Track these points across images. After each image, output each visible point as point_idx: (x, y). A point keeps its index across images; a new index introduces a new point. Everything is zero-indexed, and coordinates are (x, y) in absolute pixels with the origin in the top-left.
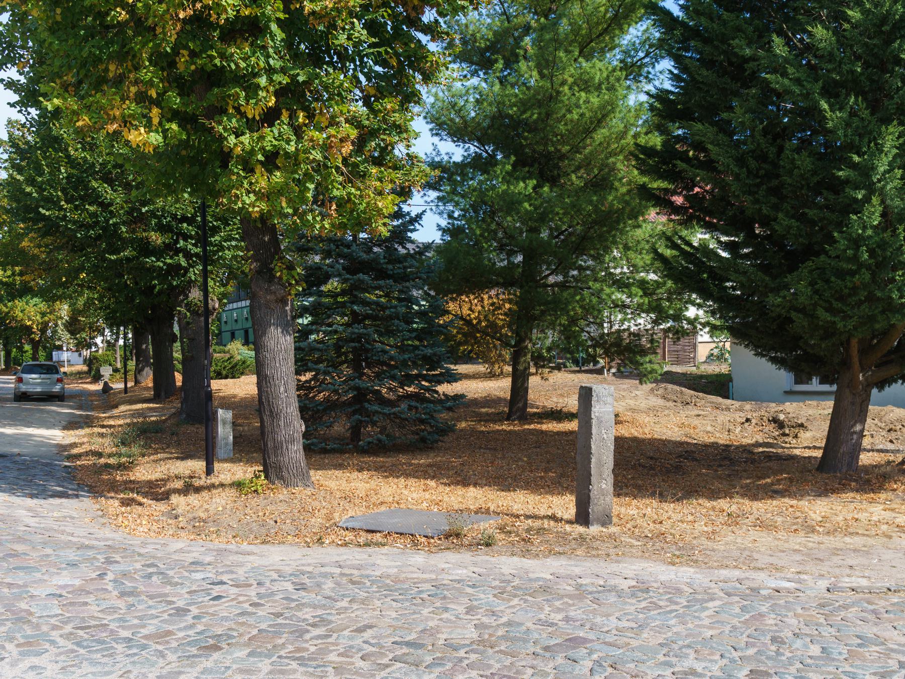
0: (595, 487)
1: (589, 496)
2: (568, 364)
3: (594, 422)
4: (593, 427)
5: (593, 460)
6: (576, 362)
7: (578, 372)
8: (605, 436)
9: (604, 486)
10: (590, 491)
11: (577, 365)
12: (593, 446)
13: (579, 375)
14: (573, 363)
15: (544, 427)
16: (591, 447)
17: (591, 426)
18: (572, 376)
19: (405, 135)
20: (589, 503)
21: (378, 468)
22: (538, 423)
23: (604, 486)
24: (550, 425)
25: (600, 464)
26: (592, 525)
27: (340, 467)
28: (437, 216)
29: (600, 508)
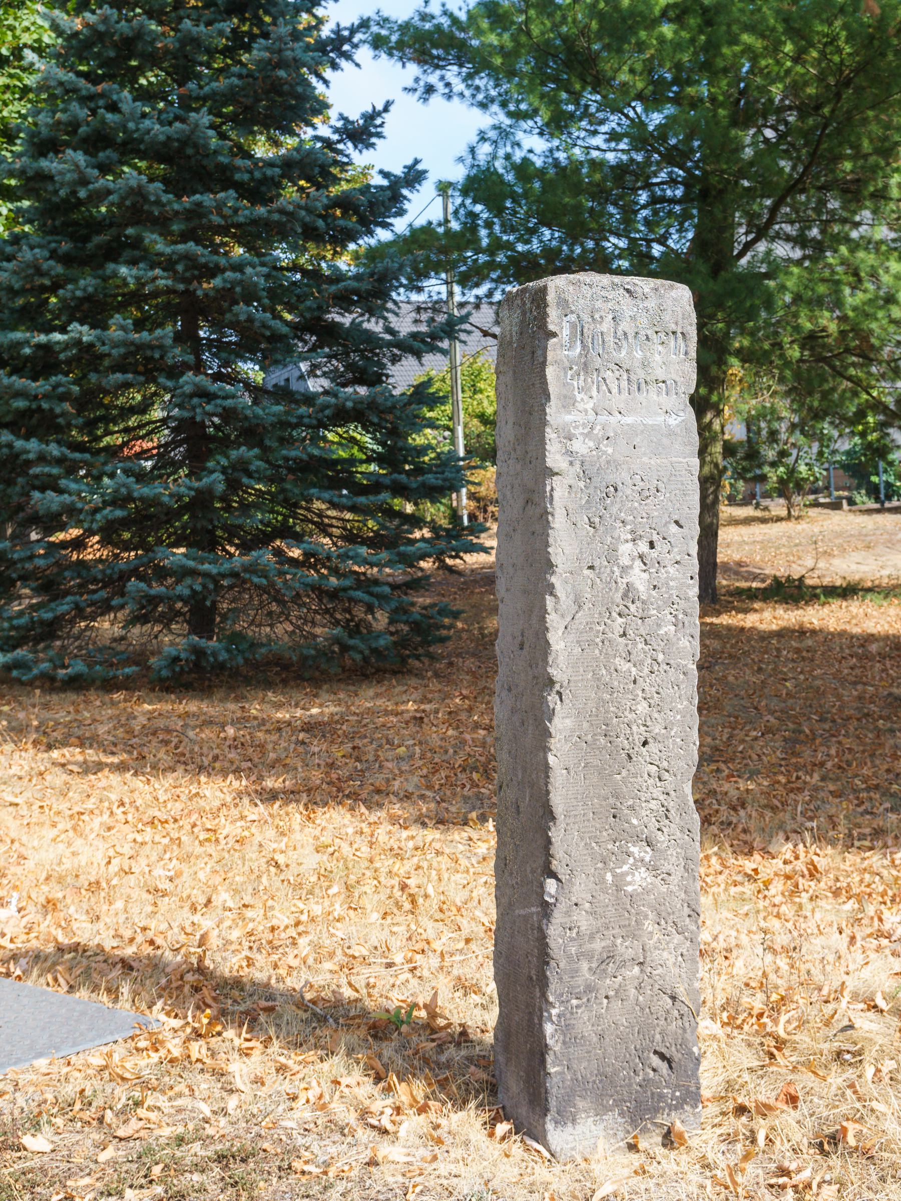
0: (580, 889)
1: (542, 938)
2: (858, 499)
3: (561, 493)
4: (559, 522)
5: (562, 725)
6: (873, 491)
7: (878, 511)
8: (639, 578)
9: (638, 880)
10: (546, 909)
11: (877, 499)
12: (557, 640)
13: (879, 518)
14: (868, 494)
15: (750, 620)
16: (545, 647)
17: (544, 518)
18: (865, 518)
19: (525, 65)
20: (543, 983)
21: (247, 761)
22: (739, 611)
23: (638, 880)
24: (767, 615)
25: (611, 748)
26: (566, 1118)
27: (139, 753)
28: (476, 111)
29: (618, 1014)
